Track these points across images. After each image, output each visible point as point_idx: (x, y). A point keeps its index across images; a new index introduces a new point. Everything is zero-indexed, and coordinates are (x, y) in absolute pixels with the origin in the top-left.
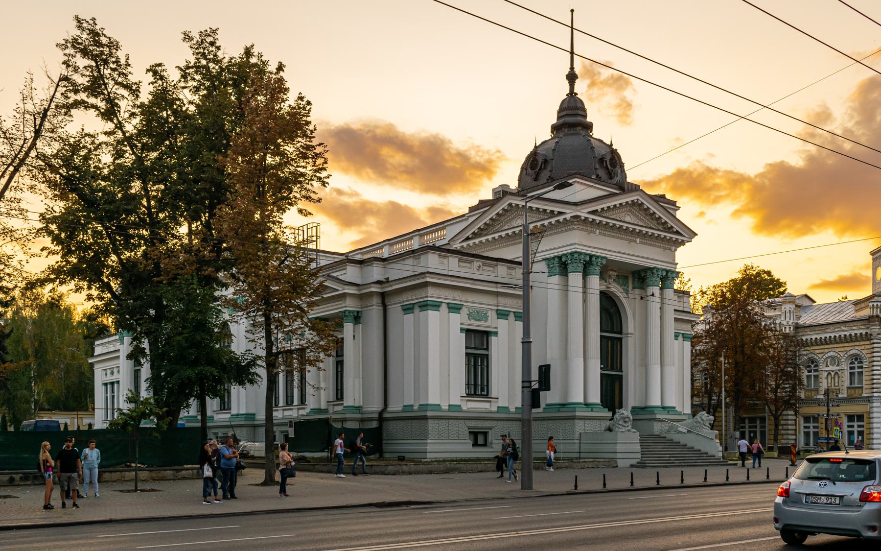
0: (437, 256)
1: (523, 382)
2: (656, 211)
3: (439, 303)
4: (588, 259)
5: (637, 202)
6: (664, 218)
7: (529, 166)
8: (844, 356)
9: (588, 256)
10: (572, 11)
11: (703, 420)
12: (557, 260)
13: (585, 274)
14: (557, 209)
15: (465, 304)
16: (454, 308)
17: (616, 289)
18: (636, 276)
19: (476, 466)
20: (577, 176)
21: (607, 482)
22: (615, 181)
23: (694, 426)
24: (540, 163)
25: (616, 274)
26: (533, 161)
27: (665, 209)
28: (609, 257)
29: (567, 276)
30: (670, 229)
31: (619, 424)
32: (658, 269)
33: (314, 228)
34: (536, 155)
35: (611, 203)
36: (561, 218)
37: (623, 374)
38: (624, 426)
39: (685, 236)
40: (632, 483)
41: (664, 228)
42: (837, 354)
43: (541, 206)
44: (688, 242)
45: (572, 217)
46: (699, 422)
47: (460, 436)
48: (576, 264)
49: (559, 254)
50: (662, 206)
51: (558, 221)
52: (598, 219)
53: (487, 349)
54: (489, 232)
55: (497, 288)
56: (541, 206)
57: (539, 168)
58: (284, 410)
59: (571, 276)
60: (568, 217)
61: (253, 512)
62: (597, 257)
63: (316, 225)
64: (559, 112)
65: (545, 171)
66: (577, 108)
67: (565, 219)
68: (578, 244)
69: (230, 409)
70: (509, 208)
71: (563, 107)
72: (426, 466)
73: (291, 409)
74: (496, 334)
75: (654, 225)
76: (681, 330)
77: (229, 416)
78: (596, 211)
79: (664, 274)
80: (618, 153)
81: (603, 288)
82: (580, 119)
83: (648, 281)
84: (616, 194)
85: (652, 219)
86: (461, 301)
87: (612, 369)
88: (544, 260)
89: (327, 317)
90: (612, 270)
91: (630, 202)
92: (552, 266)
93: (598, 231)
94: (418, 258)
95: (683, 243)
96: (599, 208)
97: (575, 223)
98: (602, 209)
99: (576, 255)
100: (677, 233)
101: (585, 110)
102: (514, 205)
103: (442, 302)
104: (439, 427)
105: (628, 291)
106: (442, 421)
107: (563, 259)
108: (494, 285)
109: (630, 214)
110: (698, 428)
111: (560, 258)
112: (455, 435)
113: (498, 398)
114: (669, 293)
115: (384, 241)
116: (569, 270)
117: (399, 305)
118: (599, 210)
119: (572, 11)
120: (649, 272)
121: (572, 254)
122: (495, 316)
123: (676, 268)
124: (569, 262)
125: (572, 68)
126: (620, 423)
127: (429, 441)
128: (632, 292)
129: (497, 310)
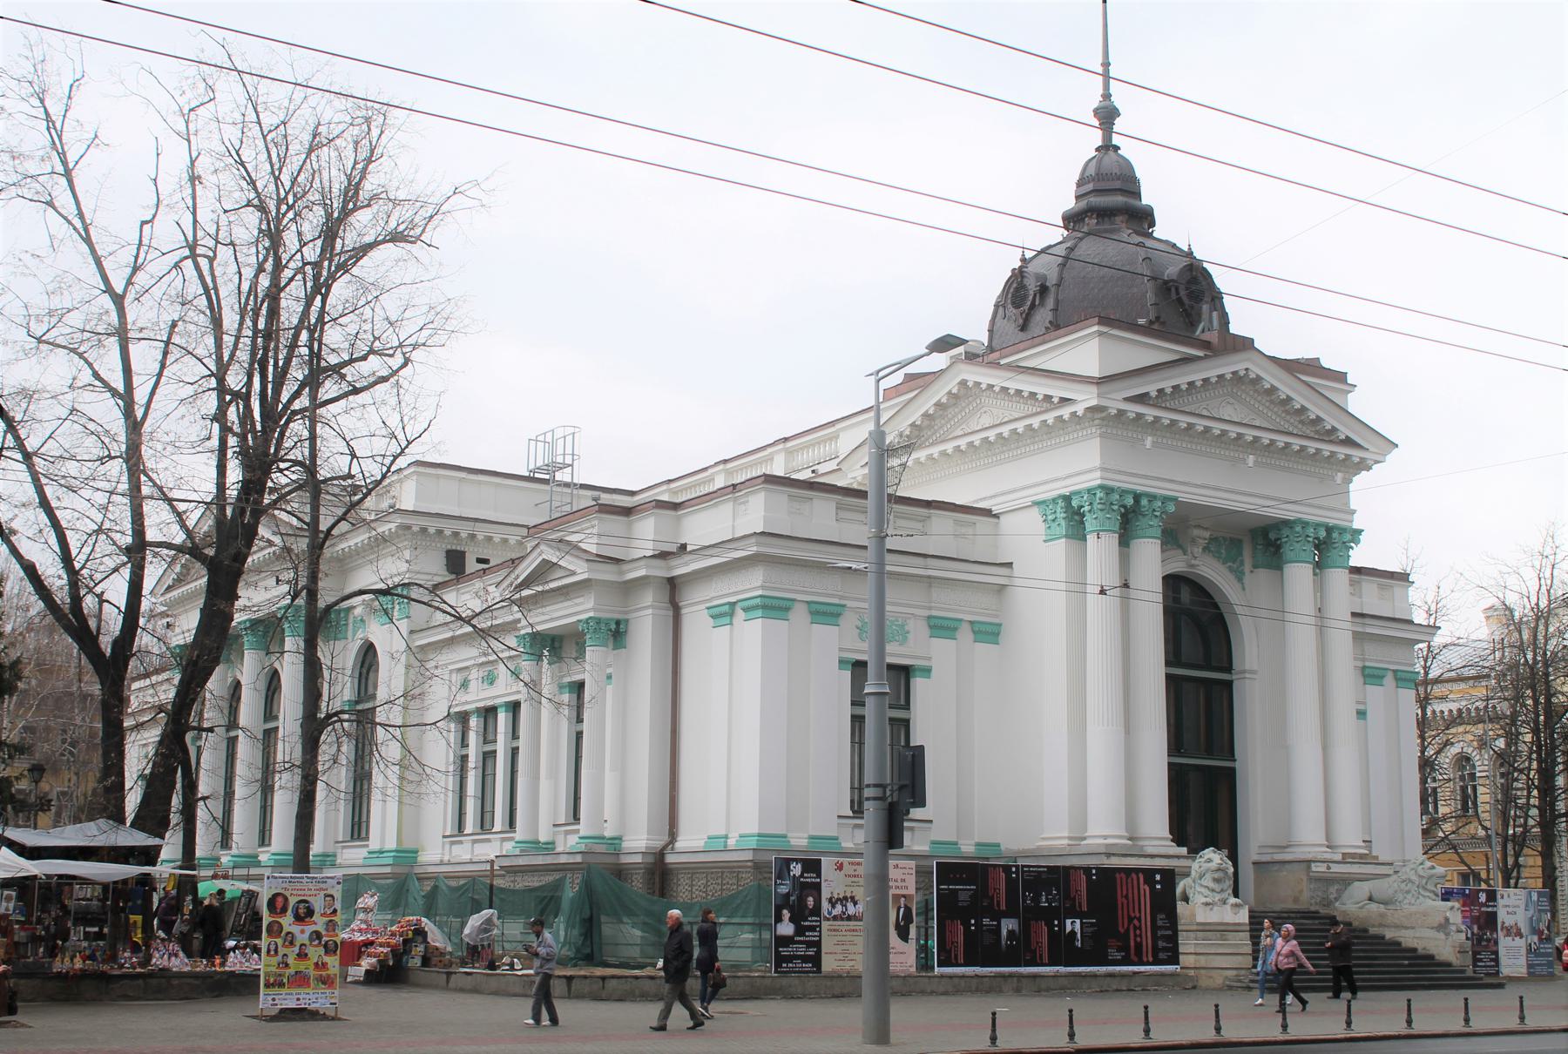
0: (785, 498)
2: (1293, 395)
3: (788, 603)
4: (1130, 501)
5: (1246, 375)
6: (1315, 411)
7: (1009, 301)
12: (1061, 503)
13: (1126, 536)
14: (1057, 390)
15: (849, 603)
16: (825, 614)
17: (1212, 572)
19: (829, 983)
24: (1032, 293)
25: (1207, 534)
26: (1017, 290)
27: (1309, 386)
28: (1183, 497)
29: (1085, 540)
30: (1330, 435)
32: (1305, 524)
33: (569, 439)
35: (1182, 378)
36: (1066, 412)
37: (1237, 765)
43: (1027, 384)
44: (1377, 462)
51: (1060, 419)
52: (1150, 413)
53: (907, 706)
56: (1027, 384)
57: (1029, 303)
58: (475, 841)
60: (1080, 409)
62: (1152, 498)
63: (572, 430)
64: (1080, 184)
65: (1042, 310)
67: (1074, 414)
69: (367, 838)
70: (962, 392)
71: (1087, 174)
73: (488, 840)
74: (927, 671)
76: (1389, 662)
77: (363, 852)
79: (1322, 534)
81: (1178, 566)
83: (1286, 549)
84: (1198, 358)
86: (841, 598)
87: (1209, 752)
88: (1037, 503)
89: (555, 633)
90: (1199, 526)
91: (1229, 376)
93: (1149, 438)
94: (744, 503)
95: (1363, 466)
96: (1152, 389)
98: (1160, 391)
100: (1349, 442)
102: (970, 384)
103: (794, 600)
107: (1075, 503)
109: (1232, 400)
111: (1067, 499)
113: (931, 821)
114: (1338, 579)
115: (717, 464)
117: (703, 606)
118: (1154, 394)
120: (1286, 532)
122: (927, 632)
123: (1352, 521)
124: (1087, 508)
125: (1107, 96)
129: (929, 617)
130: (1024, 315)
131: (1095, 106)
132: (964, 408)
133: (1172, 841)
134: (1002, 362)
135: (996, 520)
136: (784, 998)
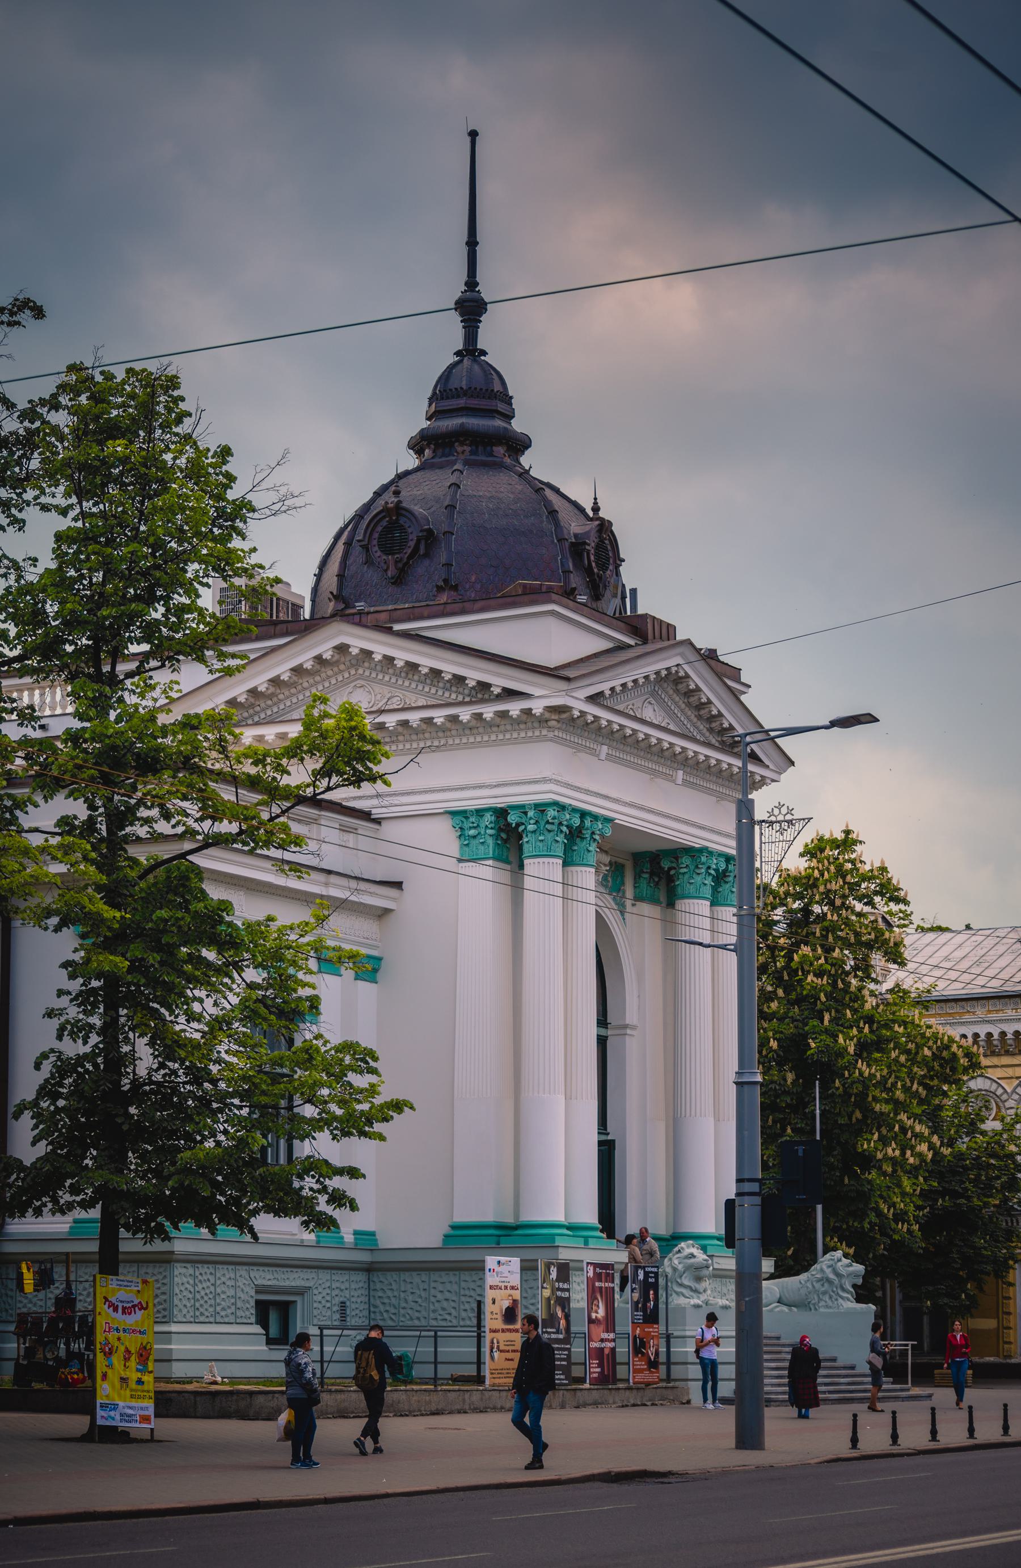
1: (739, 1181)
8: (1014, 1091)
9: (578, 815)
10: (473, 134)
11: (838, 1275)
12: (489, 818)
14: (499, 679)
18: (647, 868)
20: (554, 596)
21: (900, 1431)
22: (611, 605)
23: (816, 1291)
24: (413, 537)
28: (621, 820)
31: (681, 1285)
32: (710, 853)
34: (399, 515)
36: (515, 708)
38: (696, 1291)
39: (768, 767)
40: (1006, 1428)
41: (723, 742)
42: (994, 1086)
43: (427, 659)
44: (773, 781)
45: (550, 709)
46: (829, 1281)
47: (239, 1313)
48: (550, 836)
49: (500, 803)
50: (729, 688)
54: (251, 716)
55: (326, 884)
59: (531, 866)
60: (537, 707)
61: (325, 1499)
65: (427, 562)
66: (492, 395)
67: (528, 712)
68: (557, 782)
72: (333, 1396)
75: (700, 732)
78: (601, 694)
80: (612, 532)
82: (498, 423)
85: (700, 717)
88: (453, 813)
92: (472, 832)
93: (605, 748)
96: (605, 687)
97: (552, 723)
99: (551, 813)
101: (508, 400)
104: (195, 1285)
105: (624, 906)
106: (435, 1276)
108: (321, 877)
109: (653, 702)
110: (826, 1298)
111: (501, 813)
112: (229, 1311)
116: (527, 849)
119: (473, 134)
120: (686, 860)
121: (541, 808)
125: (472, 283)
126: (686, 1282)
127: (174, 1328)
128: (635, 910)
130: (400, 565)
131: (456, 298)
132: (329, 677)
133: (602, 1231)
134: (397, 627)
135: (377, 827)
136: (395, 1415)
